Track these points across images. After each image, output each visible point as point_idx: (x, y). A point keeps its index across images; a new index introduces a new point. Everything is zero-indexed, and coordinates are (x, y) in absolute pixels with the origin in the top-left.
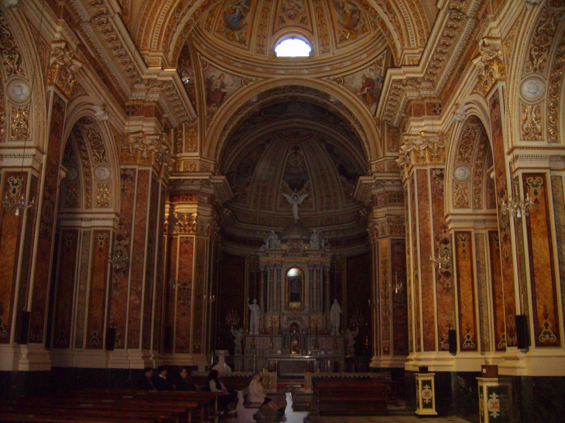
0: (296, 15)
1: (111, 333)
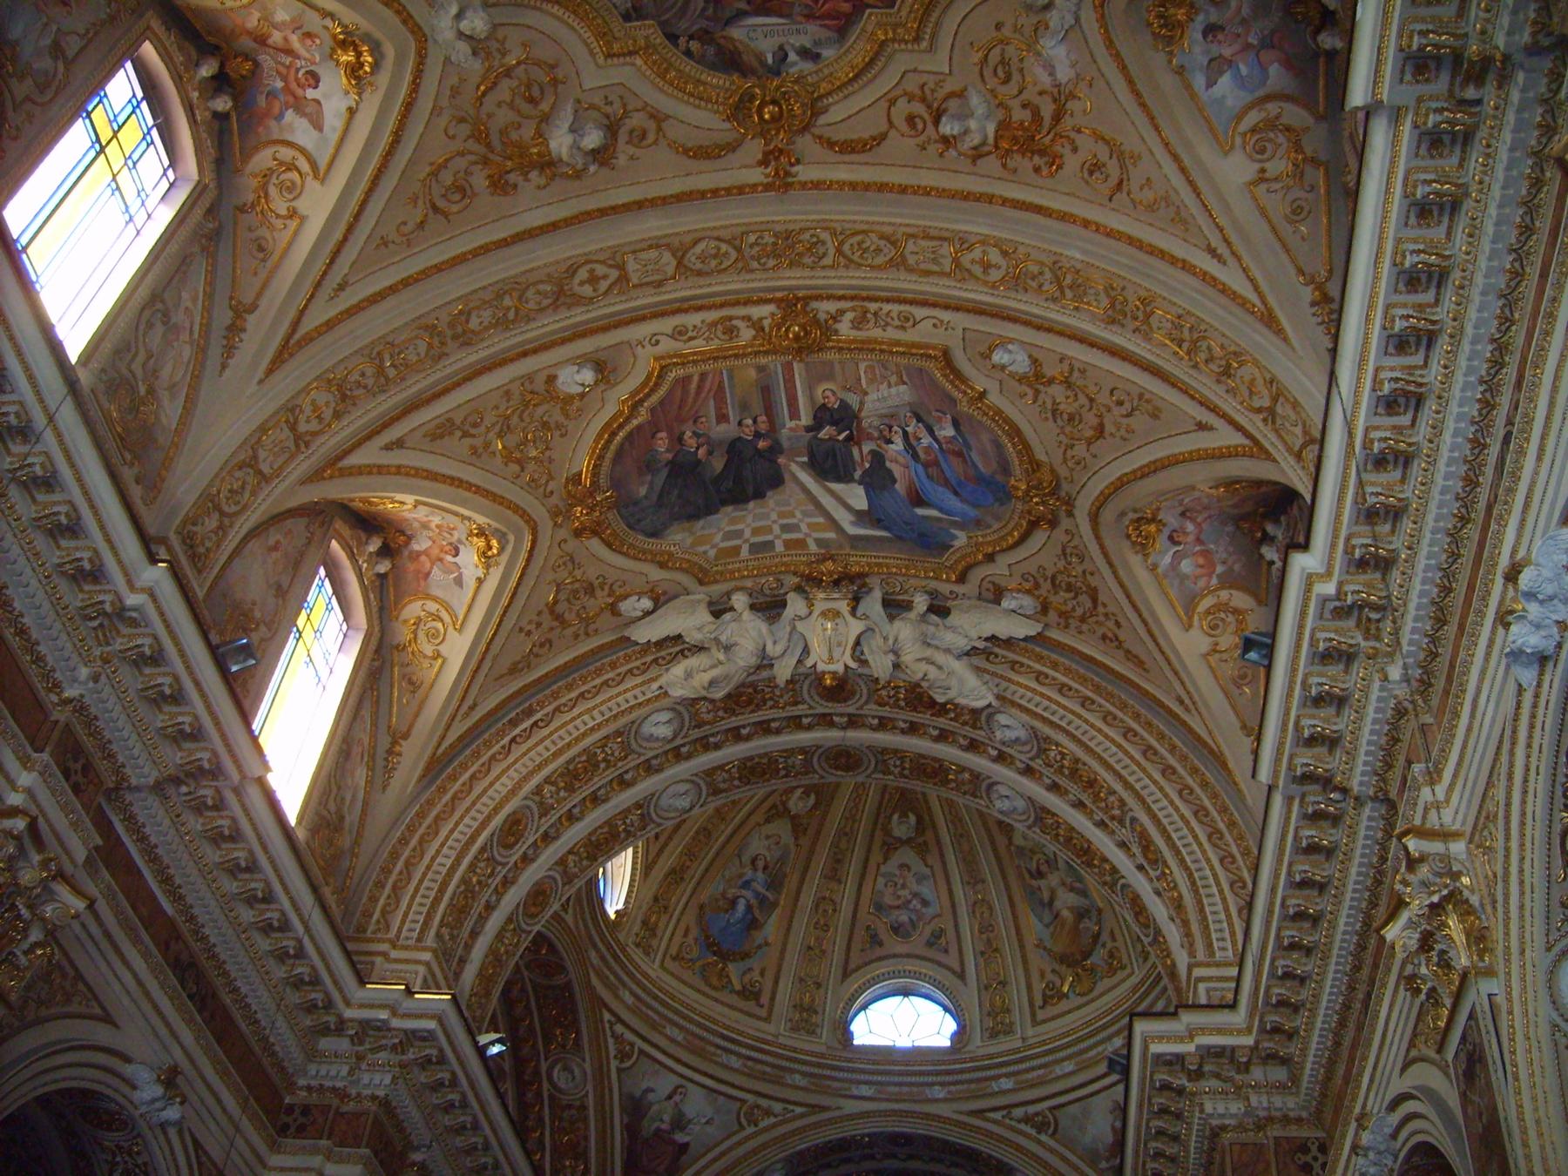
0: (913, 924)
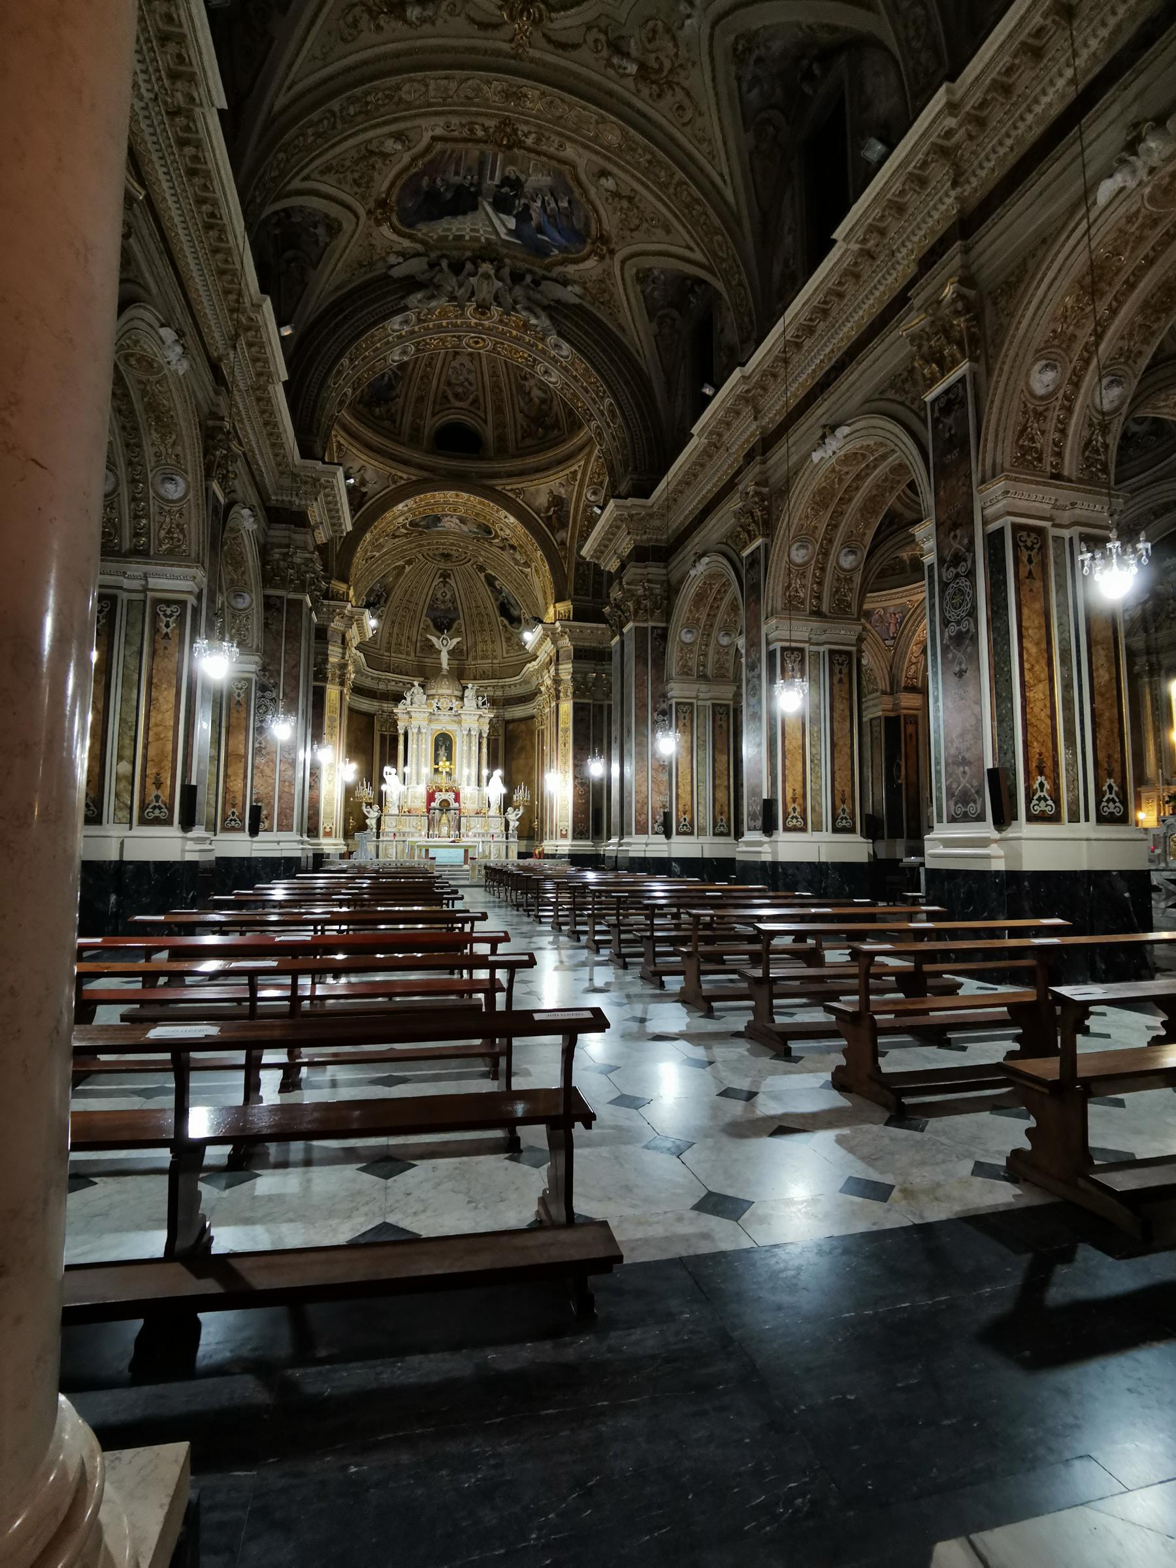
1: (256, 812)
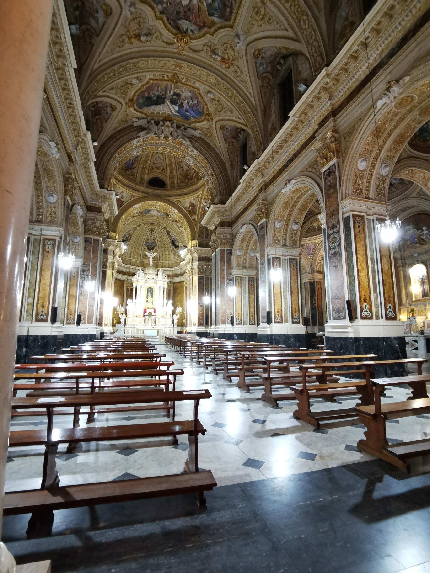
1: (79, 317)
